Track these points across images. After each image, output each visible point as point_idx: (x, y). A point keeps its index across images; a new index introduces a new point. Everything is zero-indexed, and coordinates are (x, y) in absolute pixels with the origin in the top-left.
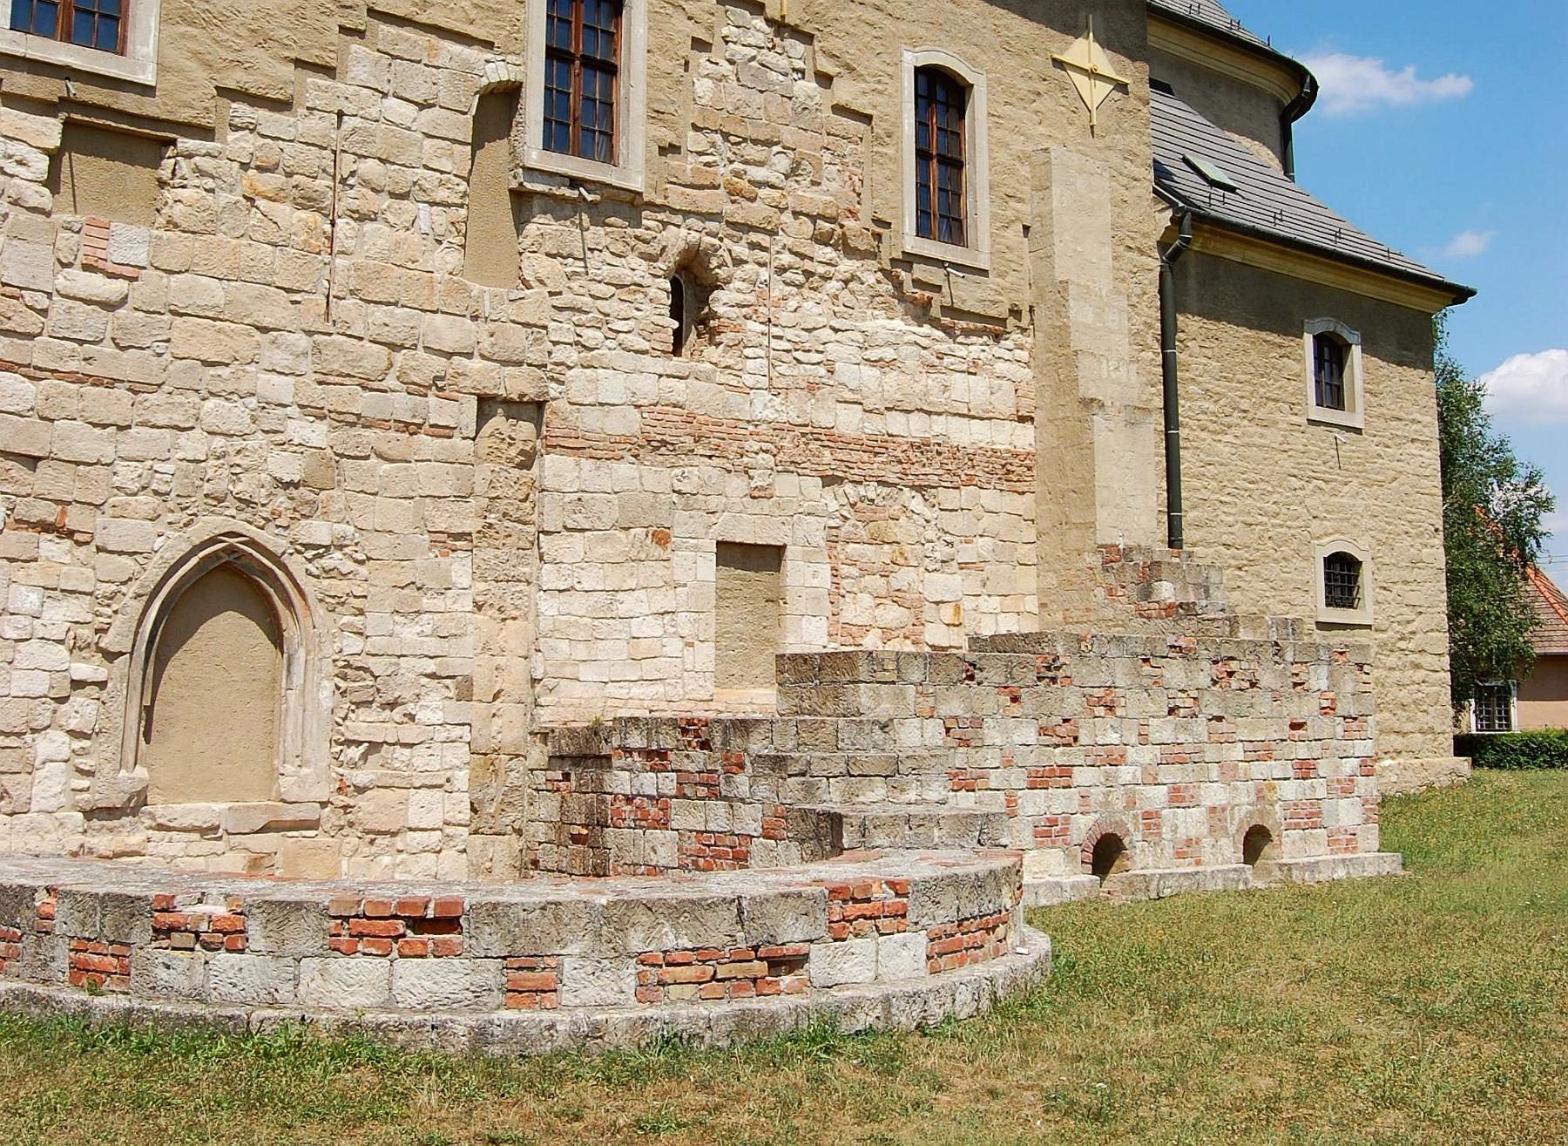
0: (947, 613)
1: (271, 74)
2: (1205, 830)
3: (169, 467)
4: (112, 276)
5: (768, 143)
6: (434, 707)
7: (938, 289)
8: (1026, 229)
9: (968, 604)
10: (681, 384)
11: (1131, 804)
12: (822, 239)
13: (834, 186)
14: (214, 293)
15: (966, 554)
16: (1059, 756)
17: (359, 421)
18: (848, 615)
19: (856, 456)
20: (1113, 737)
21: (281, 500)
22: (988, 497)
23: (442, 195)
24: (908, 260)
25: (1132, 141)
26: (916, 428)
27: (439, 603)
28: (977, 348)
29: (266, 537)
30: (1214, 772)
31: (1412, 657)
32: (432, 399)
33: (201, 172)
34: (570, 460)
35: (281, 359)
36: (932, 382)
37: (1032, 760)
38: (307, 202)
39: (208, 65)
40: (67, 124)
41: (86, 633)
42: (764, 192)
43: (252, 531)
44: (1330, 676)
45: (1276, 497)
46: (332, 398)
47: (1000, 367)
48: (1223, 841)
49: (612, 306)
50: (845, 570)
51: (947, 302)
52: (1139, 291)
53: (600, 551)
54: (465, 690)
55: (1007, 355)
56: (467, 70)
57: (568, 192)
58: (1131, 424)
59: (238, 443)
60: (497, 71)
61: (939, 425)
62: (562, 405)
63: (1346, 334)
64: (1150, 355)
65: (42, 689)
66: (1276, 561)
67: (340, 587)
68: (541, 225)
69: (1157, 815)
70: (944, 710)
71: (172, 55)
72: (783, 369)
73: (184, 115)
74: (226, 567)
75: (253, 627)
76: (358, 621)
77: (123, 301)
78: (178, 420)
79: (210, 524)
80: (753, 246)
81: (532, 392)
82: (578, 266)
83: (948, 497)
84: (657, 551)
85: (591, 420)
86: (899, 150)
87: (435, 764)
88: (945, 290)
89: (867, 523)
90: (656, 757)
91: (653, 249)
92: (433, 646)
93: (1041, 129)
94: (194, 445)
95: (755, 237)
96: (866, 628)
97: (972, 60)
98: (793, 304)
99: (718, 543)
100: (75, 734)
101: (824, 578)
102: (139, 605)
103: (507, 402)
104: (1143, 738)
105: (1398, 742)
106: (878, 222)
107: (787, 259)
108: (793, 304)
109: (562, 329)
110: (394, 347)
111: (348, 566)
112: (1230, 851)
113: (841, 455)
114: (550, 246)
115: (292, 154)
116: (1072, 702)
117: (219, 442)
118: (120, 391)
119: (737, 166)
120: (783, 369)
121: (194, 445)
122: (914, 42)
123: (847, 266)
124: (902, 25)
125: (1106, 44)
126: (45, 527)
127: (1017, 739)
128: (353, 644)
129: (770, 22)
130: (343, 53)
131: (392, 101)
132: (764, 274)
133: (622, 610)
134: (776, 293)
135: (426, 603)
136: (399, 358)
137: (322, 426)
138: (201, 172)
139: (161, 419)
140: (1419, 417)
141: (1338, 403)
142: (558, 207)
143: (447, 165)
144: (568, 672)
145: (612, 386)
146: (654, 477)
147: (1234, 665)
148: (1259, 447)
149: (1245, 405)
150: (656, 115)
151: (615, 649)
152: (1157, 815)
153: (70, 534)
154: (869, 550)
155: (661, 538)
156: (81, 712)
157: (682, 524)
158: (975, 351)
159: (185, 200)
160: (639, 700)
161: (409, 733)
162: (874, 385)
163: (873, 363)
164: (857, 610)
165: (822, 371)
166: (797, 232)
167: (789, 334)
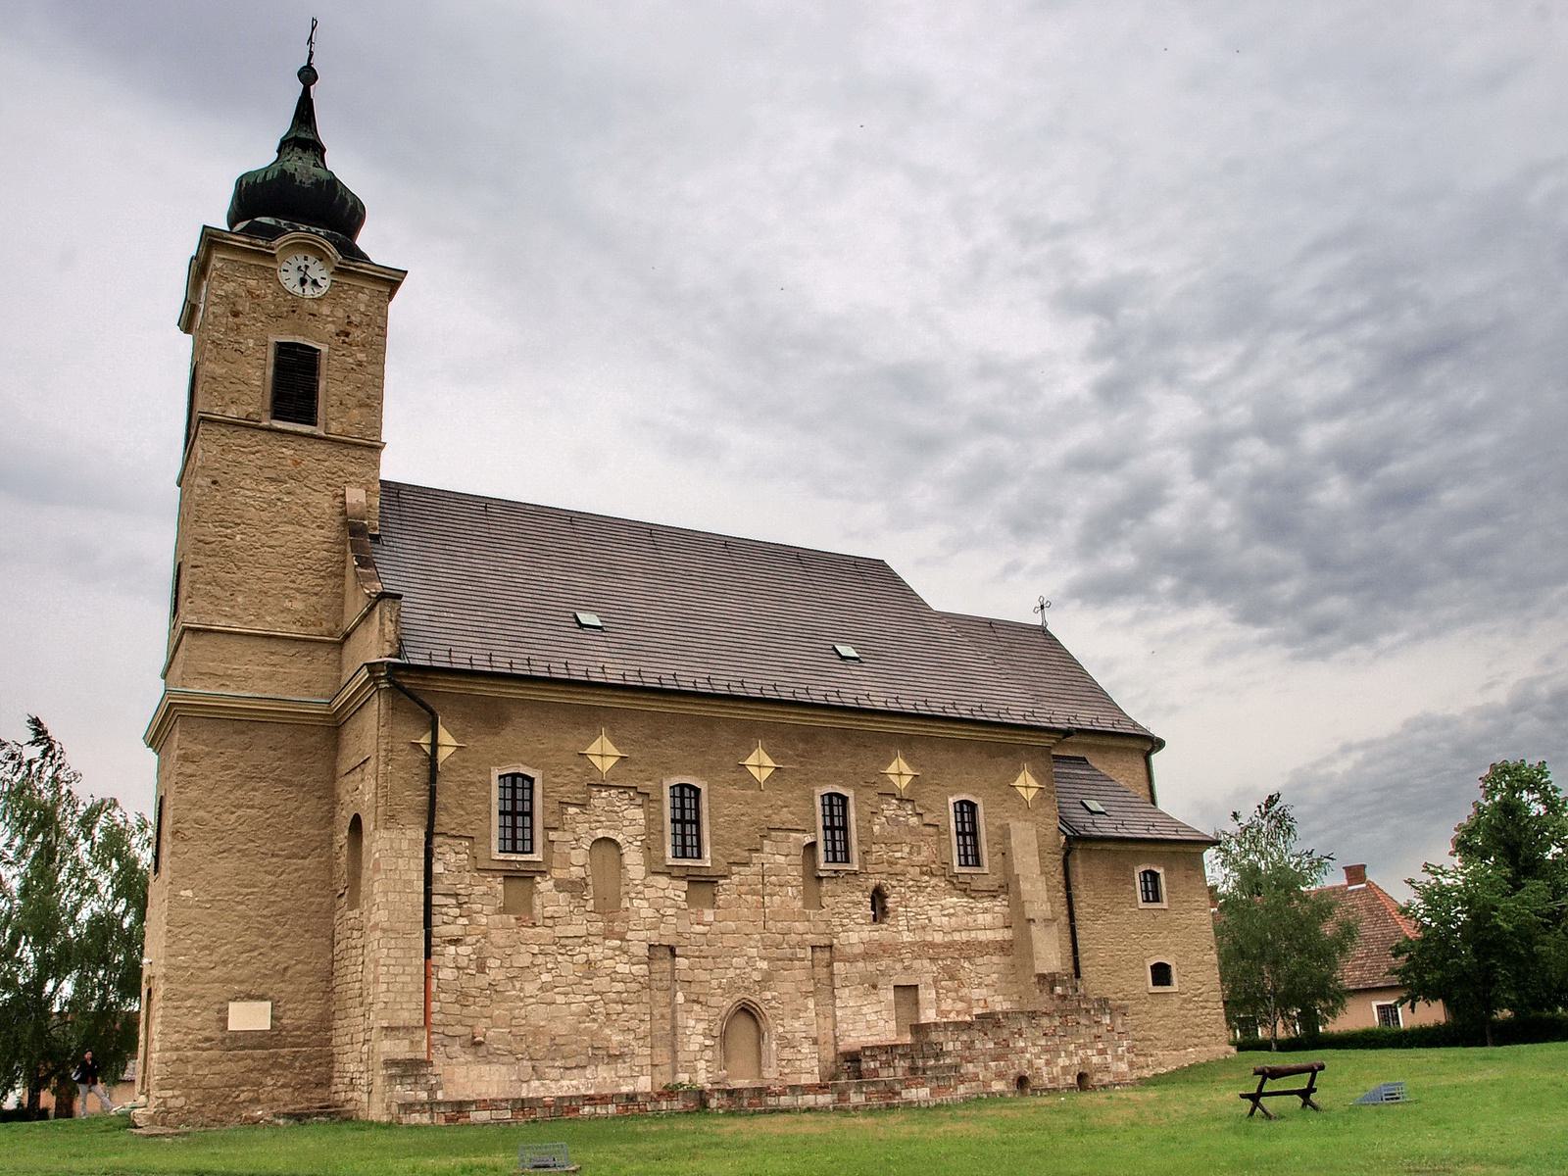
0: (982, 1003)
4: (704, 925)
6: (806, 1048)
8: (1003, 854)
9: (989, 999)
10: (877, 933)
12: (923, 873)
18: (943, 1007)
23: (795, 883)
24: (956, 876)
26: (965, 936)
27: (805, 1015)
31: (1201, 1004)
35: (752, 943)
36: (970, 919)
39: (723, 857)
40: (689, 882)
42: (901, 861)
49: (852, 910)
54: (815, 1042)
55: (999, 904)
58: (1046, 926)
59: (743, 971)
60: (808, 839)
61: (973, 934)
63: (1155, 870)
67: (775, 1011)
71: (715, 856)
72: (912, 923)
79: (738, 996)
81: (827, 942)
83: (979, 961)
86: (950, 836)
87: (808, 1066)
90: (874, 1058)
92: (804, 1028)
93: (1007, 814)
96: (950, 1012)
97: (975, 795)
98: (914, 899)
99: (895, 986)
100: (707, 1061)
101: (933, 995)
104: (1034, 1045)
105: (1196, 1041)
108: (914, 899)
116: (1005, 1033)
117: (738, 971)
119: (890, 854)
120: (912, 923)
121: (731, 973)
123: (934, 881)
126: (694, 1001)
128: (781, 1030)
130: (762, 844)
131: (777, 856)
135: (801, 1015)
136: (786, 937)
137: (766, 963)
139: (722, 966)
141: (1157, 899)
144: (847, 1033)
148: (1116, 924)
149: (1107, 907)
150: (860, 842)
151: (861, 1025)
154: (949, 983)
155: (874, 987)
158: (986, 904)
160: (873, 1040)
161: (800, 1057)
163: (944, 915)
164: (947, 1005)
167: (913, 910)
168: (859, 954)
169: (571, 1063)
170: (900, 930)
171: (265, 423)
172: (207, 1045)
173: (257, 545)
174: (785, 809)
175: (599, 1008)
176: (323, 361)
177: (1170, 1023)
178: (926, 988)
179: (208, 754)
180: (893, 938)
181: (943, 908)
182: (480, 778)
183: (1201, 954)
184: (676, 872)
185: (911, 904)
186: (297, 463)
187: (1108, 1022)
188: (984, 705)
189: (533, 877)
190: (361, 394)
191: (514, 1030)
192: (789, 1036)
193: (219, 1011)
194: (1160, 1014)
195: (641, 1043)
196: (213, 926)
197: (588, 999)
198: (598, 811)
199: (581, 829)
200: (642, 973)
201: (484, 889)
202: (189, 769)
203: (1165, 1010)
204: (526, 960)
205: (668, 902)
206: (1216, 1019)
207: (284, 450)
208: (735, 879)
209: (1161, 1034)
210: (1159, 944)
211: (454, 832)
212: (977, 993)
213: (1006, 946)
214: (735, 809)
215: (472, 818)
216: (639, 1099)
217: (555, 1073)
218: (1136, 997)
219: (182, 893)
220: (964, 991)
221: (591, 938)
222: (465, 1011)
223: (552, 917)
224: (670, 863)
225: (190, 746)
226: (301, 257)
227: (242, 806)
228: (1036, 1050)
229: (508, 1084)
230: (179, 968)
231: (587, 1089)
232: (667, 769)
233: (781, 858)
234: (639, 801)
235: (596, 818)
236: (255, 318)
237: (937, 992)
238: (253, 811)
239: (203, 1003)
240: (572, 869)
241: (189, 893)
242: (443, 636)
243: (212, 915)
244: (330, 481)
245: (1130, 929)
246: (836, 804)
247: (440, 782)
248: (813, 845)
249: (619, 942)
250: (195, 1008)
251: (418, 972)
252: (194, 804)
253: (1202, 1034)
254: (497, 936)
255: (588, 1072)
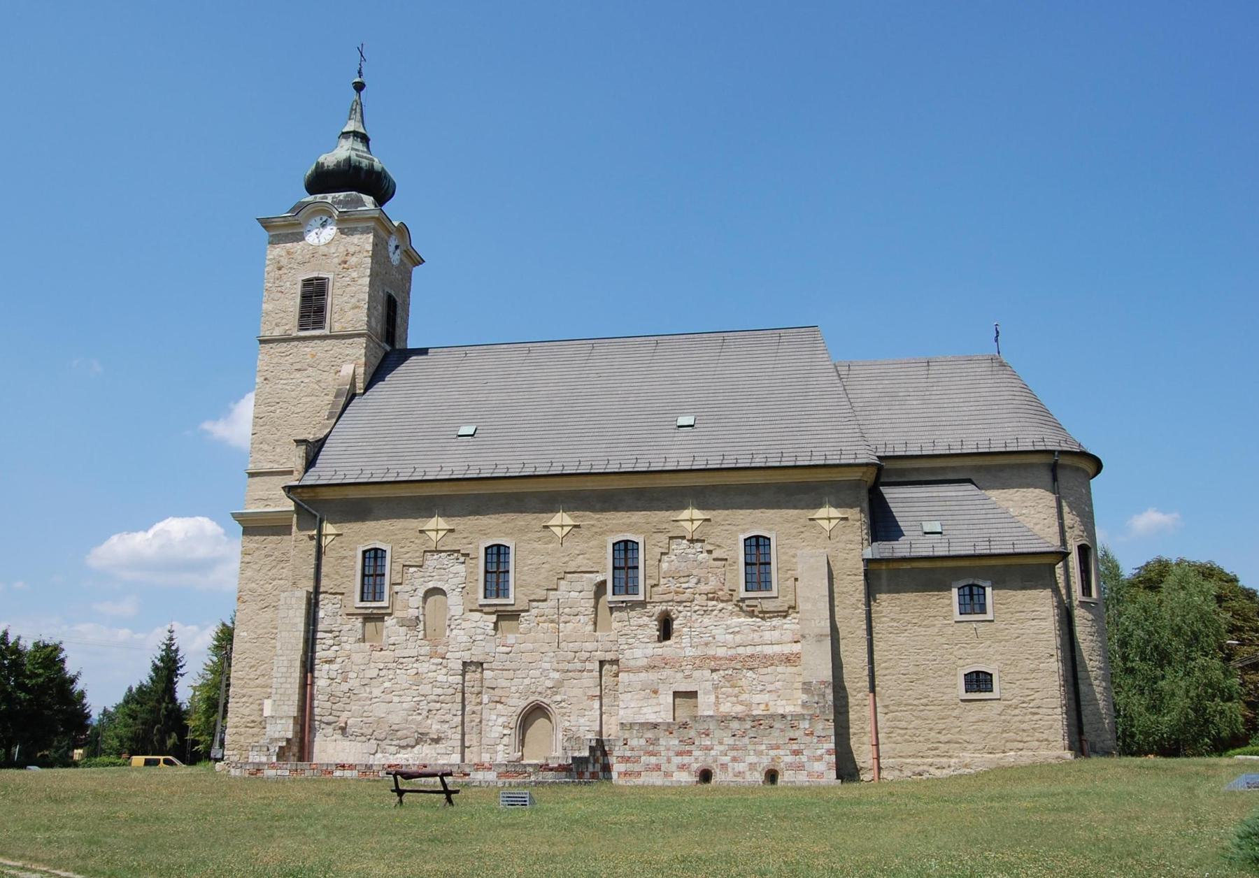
1: (541, 593)
2: (747, 769)
3: (522, 687)
5: (689, 576)
7: (756, 606)
9: (771, 703)
10: (661, 650)
11: (715, 761)
13: (713, 583)
14: (530, 646)
15: (770, 687)
16: (687, 748)
17: (568, 671)
19: (723, 662)
20: (709, 743)
21: (549, 692)
22: (780, 669)
23: (586, 613)
24: (743, 600)
25: (851, 537)
27: (590, 713)
28: (775, 622)
29: (545, 700)
30: (752, 753)
32: (587, 663)
33: (526, 620)
34: (626, 674)
36: (756, 635)
37: (676, 749)
38: (552, 622)
41: (506, 724)
43: (542, 699)
44: (810, 723)
45: (934, 653)
46: (561, 666)
47: (785, 626)
48: (755, 773)
50: (720, 696)
51: (760, 609)
52: (854, 589)
53: (636, 697)
56: (591, 579)
57: (621, 605)
60: (600, 578)
61: (759, 648)
62: (624, 660)
64: (860, 611)
65: (497, 736)
66: (935, 678)
67: (564, 710)
68: (615, 614)
69: (727, 764)
70: (646, 736)
72: (695, 640)
73: (521, 609)
74: (538, 708)
75: (546, 720)
76: (569, 719)
77: (511, 652)
78: (524, 676)
79: (532, 699)
80: (685, 607)
81: (614, 658)
82: (627, 623)
84: (654, 695)
85: (632, 663)
88: (759, 606)
89: (729, 681)
91: (651, 614)
92: (588, 723)
94: (527, 681)
95: (685, 604)
98: (699, 621)
100: (505, 745)
101: (712, 698)
102: (516, 718)
103: (608, 661)
104: (721, 743)
105: (1020, 745)
106: (731, 590)
107: (697, 608)
109: (622, 640)
110: (576, 652)
111: (566, 705)
112: (759, 777)
113: (718, 663)
114: (618, 620)
115: (547, 611)
116: (692, 733)
117: (533, 680)
118: (511, 671)
119: (678, 585)
121: (527, 681)
122: (744, 531)
123: (721, 605)
124: (740, 527)
125: (836, 506)
126: (497, 702)
127: (671, 743)
128: (567, 724)
129: (688, 540)
132: (689, 614)
133: (642, 712)
134: (694, 618)
135: (586, 713)
136: (577, 654)
137: (558, 673)
138: (526, 620)
140: (1037, 609)
142: (620, 609)
143: (587, 605)
145: (638, 653)
146: (653, 676)
147: (761, 722)
148: (924, 636)
152: (727, 764)
153: (502, 703)
154: (730, 690)
155: (655, 692)
156: (506, 740)
157: (661, 688)
158: (774, 623)
159: (523, 626)
162: (731, 640)
165: (711, 638)
166: (700, 599)
167: (698, 630)
168: (643, 667)
169: (403, 743)
170: (682, 645)
171: (294, 335)
172: (252, 725)
173: (289, 414)
174: (581, 556)
175: (423, 705)
176: (331, 284)
177: (986, 727)
178: (705, 694)
179: (257, 548)
180: (676, 652)
181: (728, 627)
182: (351, 553)
183: (1036, 662)
184: (486, 609)
185: (696, 625)
186: (314, 356)
187: (807, 726)
188: (813, 449)
189: (383, 618)
190: (353, 300)
191: (364, 719)
192: (573, 729)
193: (260, 704)
194: (973, 719)
195: (454, 730)
196: (257, 653)
197: (415, 699)
198: (430, 569)
199: (417, 583)
200: (456, 681)
201: (349, 626)
202: (248, 559)
203: (981, 715)
204: (374, 673)
205: (479, 631)
206: (1052, 725)
207: (306, 349)
208: (534, 612)
209: (974, 737)
210: (977, 653)
211: (332, 591)
212: (758, 698)
213: (792, 658)
214: (537, 560)
215: (344, 580)
216: (374, 768)
217: (393, 749)
218: (944, 702)
219: (242, 634)
220: (744, 697)
221: (420, 657)
222: (335, 707)
223: (394, 644)
224: (481, 603)
225: (248, 544)
226: (318, 218)
227: (275, 579)
228: (722, 748)
229: (361, 755)
230: (239, 679)
231: (414, 760)
232: (485, 534)
233: (578, 594)
234: (462, 559)
235: (428, 574)
236: (290, 268)
237: (717, 697)
238: (282, 582)
239: (251, 700)
240: (410, 610)
241: (245, 634)
242: (815, 424)
243: (257, 646)
244: (333, 363)
245: (943, 640)
246: (625, 549)
247: (324, 559)
248: (604, 583)
249: (441, 660)
250: (246, 702)
251: (295, 682)
252: (250, 580)
253: (1029, 739)
254: (357, 658)
255: (416, 750)
